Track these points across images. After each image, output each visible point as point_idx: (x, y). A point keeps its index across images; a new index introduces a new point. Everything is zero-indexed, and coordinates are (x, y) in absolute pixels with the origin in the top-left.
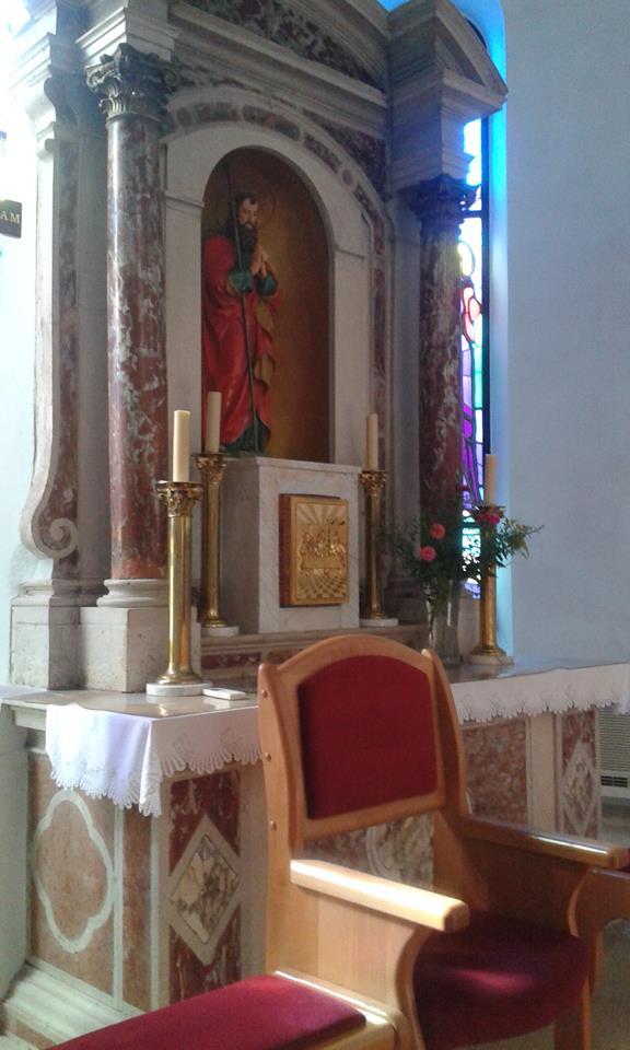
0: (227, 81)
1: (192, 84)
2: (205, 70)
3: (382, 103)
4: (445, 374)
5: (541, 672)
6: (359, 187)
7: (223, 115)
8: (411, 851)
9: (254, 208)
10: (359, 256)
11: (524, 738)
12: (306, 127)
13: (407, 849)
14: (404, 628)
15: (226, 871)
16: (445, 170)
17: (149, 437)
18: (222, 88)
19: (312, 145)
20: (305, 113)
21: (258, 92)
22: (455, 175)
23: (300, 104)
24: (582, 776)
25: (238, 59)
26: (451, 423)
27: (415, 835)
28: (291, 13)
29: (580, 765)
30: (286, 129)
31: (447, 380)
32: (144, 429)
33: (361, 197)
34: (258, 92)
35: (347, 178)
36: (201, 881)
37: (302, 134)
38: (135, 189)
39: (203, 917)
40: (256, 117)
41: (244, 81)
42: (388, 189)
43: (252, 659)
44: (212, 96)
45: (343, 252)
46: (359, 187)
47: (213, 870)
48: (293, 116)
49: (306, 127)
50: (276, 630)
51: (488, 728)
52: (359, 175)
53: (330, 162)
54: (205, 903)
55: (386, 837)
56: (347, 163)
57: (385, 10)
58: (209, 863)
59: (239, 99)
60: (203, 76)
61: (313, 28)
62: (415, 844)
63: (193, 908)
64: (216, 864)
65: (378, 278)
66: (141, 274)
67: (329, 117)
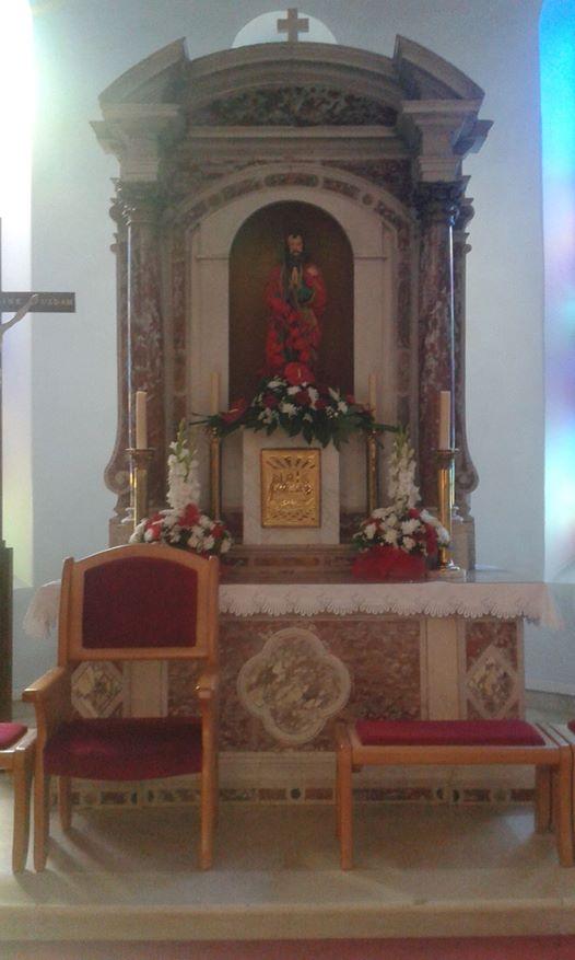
0: (251, 163)
2: (231, 162)
4: (426, 342)
8: (282, 698)
9: (298, 240)
11: (418, 635)
12: (322, 173)
13: (278, 697)
14: (343, 546)
15: (111, 681)
19: (330, 185)
20: (324, 163)
21: (277, 162)
23: (317, 158)
24: (493, 677)
26: (431, 382)
27: (286, 689)
29: (492, 665)
30: (306, 181)
31: (429, 347)
34: (277, 162)
35: (367, 200)
36: (93, 681)
37: (321, 180)
39: (94, 704)
40: (273, 181)
43: (241, 561)
45: (361, 259)
47: (102, 678)
48: (308, 170)
50: (259, 543)
51: (346, 624)
52: (381, 195)
53: (348, 192)
54: (96, 696)
55: (258, 684)
56: (364, 186)
57: (389, 59)
58: (100, 673)
60: (231, 167)
61: (335, 94)
62: (286, 695)
63: (87, 696)
64: (104, 675)
65: (404, 270)
66: (137, 321)
67: (347, 158)
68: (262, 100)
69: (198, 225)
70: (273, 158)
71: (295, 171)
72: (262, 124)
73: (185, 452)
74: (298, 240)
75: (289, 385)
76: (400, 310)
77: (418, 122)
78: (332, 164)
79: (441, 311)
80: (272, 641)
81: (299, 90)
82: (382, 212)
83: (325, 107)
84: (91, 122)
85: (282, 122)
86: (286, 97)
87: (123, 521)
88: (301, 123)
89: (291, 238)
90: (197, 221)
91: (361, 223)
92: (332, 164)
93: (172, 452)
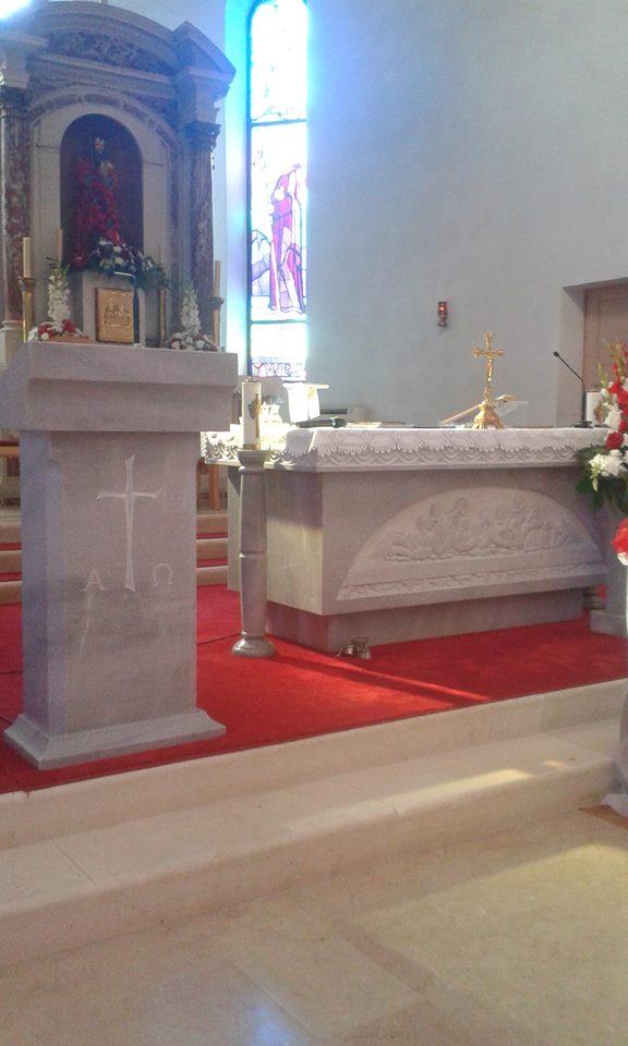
1: (55, 88)
3: (169, 83)
5: (585, 338)
6: (160, 126)
7: (70, 101)
9: (102, 142)
10: (157, 165)
12: (124, 99)
16: (199, 118)
17: (16, 258)
18: (73, 87)
22: (211, 122)
25: (79, 73)
28: (116, 40)
30: (112, 103)
32: (14, 255)
33: (160, 132)
35: (151, 123)
38: (10, 149)
40: (89, 99)
41: (85, 81)
42: (180, 127)
44: (65, 93)
45: (149, 163)
46: (160, 126)
49: (124, 99)
52: (160, 121)
53: (139, 115)
56: (151, 115)
59: (82, 92)
61: (131, 46)
68: (82, 40)
69: (39, 121)
70: (90, 82)
71: (104, 94)
72: (82, 56)
73: (60, 283)
74: (102, 142)
75: (115, 245)
76: (172, 197)
77: (196, 81)
78: (128, 94)
79: (208, 207)
80: (211, 442)
81: (107, 38)
82: (160, 133)
83: (126, 54)
84: (565, 288)
85: (95, 59)
86: (98, 41)
87: (595, 488)
88: (106, 61)
89: (98, 139)
90: (38, 119)
91: (146, 135)
92: (128, 94)
93: (50, 281)
